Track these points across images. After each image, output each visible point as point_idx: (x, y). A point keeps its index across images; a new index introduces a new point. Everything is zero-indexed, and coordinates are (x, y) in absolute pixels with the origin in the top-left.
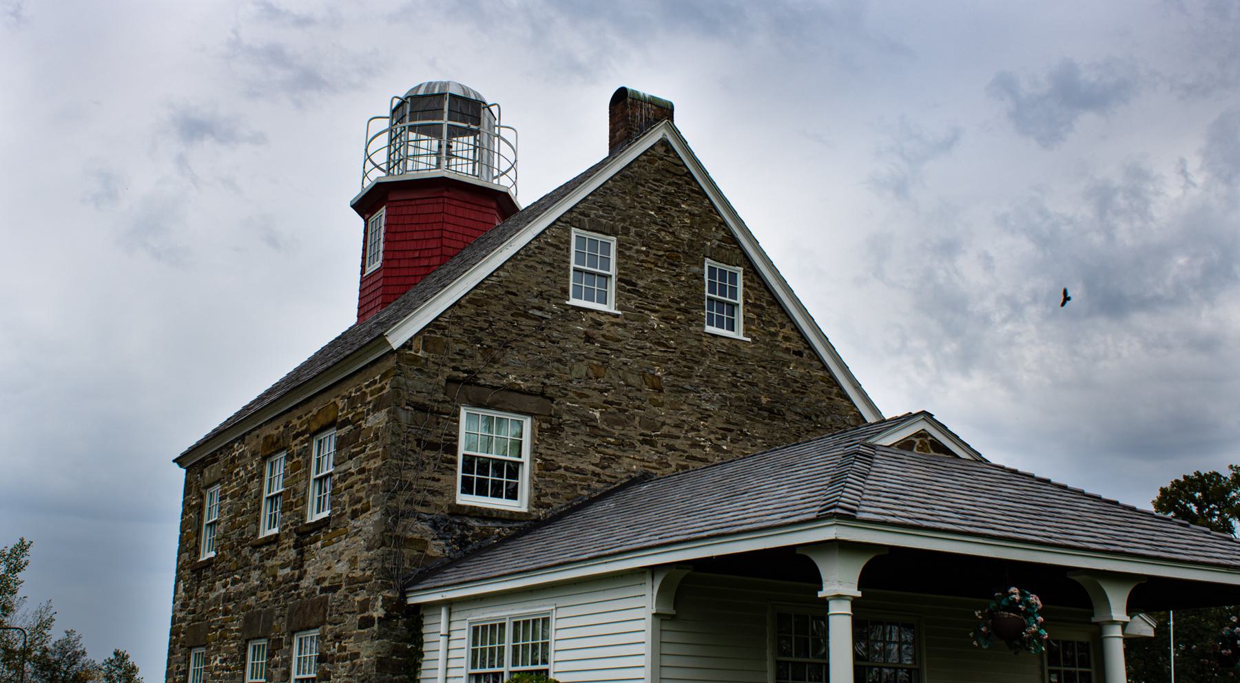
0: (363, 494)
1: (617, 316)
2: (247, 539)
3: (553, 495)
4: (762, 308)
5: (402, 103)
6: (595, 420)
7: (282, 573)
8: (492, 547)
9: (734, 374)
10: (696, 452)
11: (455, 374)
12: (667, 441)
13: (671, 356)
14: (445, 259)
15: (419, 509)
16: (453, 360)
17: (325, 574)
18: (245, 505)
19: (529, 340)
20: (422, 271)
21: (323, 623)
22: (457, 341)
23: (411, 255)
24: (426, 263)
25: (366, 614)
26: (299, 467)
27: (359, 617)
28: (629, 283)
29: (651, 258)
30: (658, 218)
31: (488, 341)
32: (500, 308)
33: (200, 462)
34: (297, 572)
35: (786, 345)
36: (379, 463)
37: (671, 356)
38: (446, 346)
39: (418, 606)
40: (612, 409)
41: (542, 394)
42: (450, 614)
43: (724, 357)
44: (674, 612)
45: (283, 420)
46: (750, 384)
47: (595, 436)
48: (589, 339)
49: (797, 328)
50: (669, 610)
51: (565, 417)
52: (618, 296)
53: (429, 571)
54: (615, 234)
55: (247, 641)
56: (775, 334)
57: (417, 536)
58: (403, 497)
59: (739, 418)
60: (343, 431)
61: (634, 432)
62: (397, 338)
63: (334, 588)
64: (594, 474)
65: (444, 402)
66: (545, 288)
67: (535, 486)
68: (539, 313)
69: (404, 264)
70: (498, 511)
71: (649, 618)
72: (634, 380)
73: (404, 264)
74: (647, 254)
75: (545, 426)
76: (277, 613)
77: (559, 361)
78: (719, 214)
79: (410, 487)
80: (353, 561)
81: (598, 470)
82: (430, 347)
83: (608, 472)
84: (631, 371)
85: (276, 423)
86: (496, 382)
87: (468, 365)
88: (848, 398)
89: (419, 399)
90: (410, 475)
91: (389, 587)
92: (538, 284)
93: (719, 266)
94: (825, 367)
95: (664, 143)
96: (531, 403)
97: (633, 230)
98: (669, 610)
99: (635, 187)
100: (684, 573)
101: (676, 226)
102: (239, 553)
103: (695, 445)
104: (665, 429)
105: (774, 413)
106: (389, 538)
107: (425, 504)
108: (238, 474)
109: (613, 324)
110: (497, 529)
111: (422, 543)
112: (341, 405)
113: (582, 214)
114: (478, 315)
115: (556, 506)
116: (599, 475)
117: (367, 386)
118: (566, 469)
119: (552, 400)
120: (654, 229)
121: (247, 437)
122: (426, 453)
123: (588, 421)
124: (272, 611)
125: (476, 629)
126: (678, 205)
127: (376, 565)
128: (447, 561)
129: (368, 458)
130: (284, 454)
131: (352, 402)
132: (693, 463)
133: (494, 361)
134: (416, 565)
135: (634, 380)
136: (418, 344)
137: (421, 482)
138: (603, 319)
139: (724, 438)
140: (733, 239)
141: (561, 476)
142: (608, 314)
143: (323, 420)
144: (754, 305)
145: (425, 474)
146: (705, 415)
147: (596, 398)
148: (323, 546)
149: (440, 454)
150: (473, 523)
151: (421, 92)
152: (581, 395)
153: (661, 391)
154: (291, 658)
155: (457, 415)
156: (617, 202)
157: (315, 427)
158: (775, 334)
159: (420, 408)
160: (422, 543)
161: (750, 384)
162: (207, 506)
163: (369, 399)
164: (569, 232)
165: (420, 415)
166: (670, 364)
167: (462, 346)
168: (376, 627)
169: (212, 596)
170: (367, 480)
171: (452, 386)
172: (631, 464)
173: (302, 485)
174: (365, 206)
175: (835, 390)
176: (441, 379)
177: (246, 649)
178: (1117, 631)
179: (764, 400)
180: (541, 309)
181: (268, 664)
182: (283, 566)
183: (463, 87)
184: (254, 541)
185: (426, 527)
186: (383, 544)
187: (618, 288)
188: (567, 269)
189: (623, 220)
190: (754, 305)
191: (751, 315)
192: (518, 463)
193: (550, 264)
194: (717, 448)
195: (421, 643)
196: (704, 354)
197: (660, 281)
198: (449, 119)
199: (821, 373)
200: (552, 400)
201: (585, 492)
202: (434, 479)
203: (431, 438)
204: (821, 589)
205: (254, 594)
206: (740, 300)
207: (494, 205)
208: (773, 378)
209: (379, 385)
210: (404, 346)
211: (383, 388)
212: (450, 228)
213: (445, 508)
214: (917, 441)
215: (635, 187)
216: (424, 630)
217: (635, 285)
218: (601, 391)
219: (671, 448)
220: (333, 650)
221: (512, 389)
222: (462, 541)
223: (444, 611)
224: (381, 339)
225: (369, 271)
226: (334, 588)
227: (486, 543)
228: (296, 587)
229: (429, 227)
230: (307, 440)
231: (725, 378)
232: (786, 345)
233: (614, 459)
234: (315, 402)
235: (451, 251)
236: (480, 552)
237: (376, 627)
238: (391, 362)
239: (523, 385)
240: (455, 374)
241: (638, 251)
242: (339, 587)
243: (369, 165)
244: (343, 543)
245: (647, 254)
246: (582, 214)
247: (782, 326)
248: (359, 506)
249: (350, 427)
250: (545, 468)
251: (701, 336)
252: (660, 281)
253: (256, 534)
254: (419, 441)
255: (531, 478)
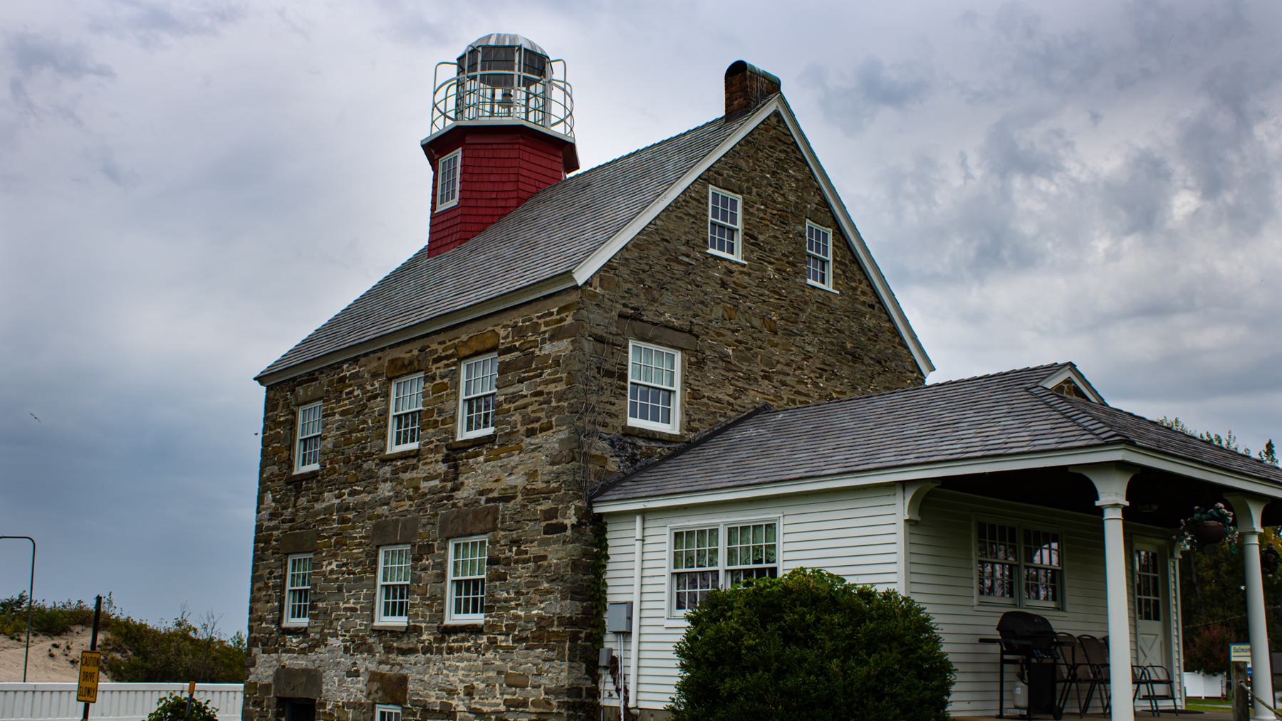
0: (542, 415)
1: (744, 266)
2: (371, 454)
3: (700, 420)
4: (845, 264)
5: (473, 51)
6: (728, 356)
7: (425, 486)
8: (655, 465)
9: (828, 322)
10: (801, 388)
11: (625, 310)
12: (781, 377)
13: (783, 303)
14: (521, 201)
15: (601, 429)
16: (623, 298)
17: (494, 486)
18: (365, 422)
19: (679, 283)
20: (500, 211)
21: (495, 529)
22: (626, 281)
23: (488, 196)
24: (503, 204)
25: (554, 521)
26: (443, 388)
27: (543, 524)
28: (752, 237)
29: (768, 217)
30: (773, 181)
31: (649, 283)
32: (656, 253)
33: (286, 385)
34: (449, 485)
35: (863, 298)
36: (561, 387)
37: (783, 303)
38: (618, 285)
39: (601, 515)
40: (741, 348)
41: (690, 332)
42: (644, 521)
43: (821, 306)
44: (918, 518)
45: (419, 344)
46: (839, 331)
47: (729, 370)
48: (724, 285)
49: (871, 285)
50: (917, 518)
51: (708, 353)
52: (744, 248)
53: (608, 486)
54: (742, 193)
55: (378, 547)
56: (855, 289)
57: (599, 453)
58: (588, 417)
59: (832, 360)
60: (508, 357)
61: (757, 369)
62: (581, 276)
63: (505, 499)
64: (730, 404)
65: (618, 334)
66: (691, 237)
67: (686, 413)
68: (686, 260)
69: (481, 203)
70: (660, 433)
71: (901, 525)
72: (757, 322)
73: (481, 203)
74: (765, 212)
75: (693, 359)
76: (424, 521)
77: (702, 303)
78: (816, 180)
79: (593, 411)
80: (532, 475)
81: (732, 400)
82: (606, 285)
83: (739, 402)
84: (754, 314)
85: (408, 347)
86: (656, 319)
87: (634, 302)
88: (906, 347)
89: (599, 331)
90: (593, 399)
91: (580, 498)
92: (685, 233)
93: (816, 226)
94: (890, 320)
95: (776, 114)
96: (682, 339)
97: (755, 190)
98: (917, 518)
99: (756, 152)
100: (933, 486)
101: (786, 189)
102: (360, 466)
103: (801, 382)
104: (779, 367)
105: (856, 358)
106: (576, 452)
107: (605, 425)
108: (351, 392)
109: (741, 273)
110: (659, 449)
111: (602, 459)
112: (502, 333)
113: (717, 173)
114: (641, 258)
115: (702, 430)
116: (731, 404)
117: (539, 318)
118: (709, 398)
119: (697, 337)
120: (770, 190)
121: (363, 360)
122: (605, 379)
123: (723, 357)
124: (415, 520)
125: (676, 534)
126: (786, 171)
127: (565, 478)
128: (622, 475)
129: (547, 383)
130: (421, 375)
131: (519, 331)
132: (800, 401)
133: (654, 300)
134: (599, 479)
135: (757, 322)
136: (596, 282)
137: (602, 405)
138: (734, 267)
139: (821, 377)
140: (828, 205)
141: (706, 404)
142: (737, 263)
143: (475, 346)
144: (840, 263)
145: (604, 398)
146: (807, 357)
147: (730, 337)
148: (486, 461)
149: (616, 382)
150: (640, 443)
151: (492, 42)
152: (719, 334)
153: (776, 333)
154: (446, 561)
155: (626, 347)
156: (743, 164)
157: (466, 352)
158: (855, 289)
159: (599, 339)
160: (602, 459)
161: (839, 331)
162: (300, 422)
163: (543, 329)
164: (707, 188)
165: (599, 345)
166: (782, 311)
167: (630, 286)
168: (569, 532)
169: (318, 506)
170: (548, 402)
171: (623, 321)
172: (754, 397)
173: (449, 405)
174: (435, 148)
175: (897, 340)
176: (614, 314)
177: (377, 555)
178: (1255, 540)
179: (849, 346)
180: (688, 256)
181: (414, 568)
182: (427, 479)
183: (530, 42)
184: (381, 455)
185: (606, 445)
186: (573, 459)
187: (744, 241)
188: (706, 221)
189: (747, 181)
190: (840, 263)
191: (838, 271)
192: (670, 391)
193: (694, 217)
194: (816, 385)
195: (606, 547)
196: (806, 303)
197: (775, 237)
198: (483, 69)
199: (887, 325)
200: (697, 337)
201: (722, 419)
202: (611, 404)
203: (607, 366)
204: (1097, 499)
205: (388, 504)
206: (830, 257)
207: (561, 154)
208: (855, 327)
209: (555, 317)
210: (586, 283)
211: (562, 320)
212: (525, 173)
213: (620, 429)
214: (1066, 386)
215: (756, 152)
216: (608, 536)
217: (756, 239)
218: (733, 331)
219: (784, 384)
220: (508, 554)
221: (667, 326)
222: (633, 459)
223: (638, 519)
224: (568, 274)
225: (440, 208)
226: (505, 499)
227: (651, 461)
228: (450, 498)
229: (505, 171)
230: (454, 364)
231: (821, 324)
232: (863, 298)
233: (743, 391)
234: (464, 329)
235: (524, 195)
236: (645, 468)
237: (569, 532)
238: (574, 297)
239: (676, 323)
240: (625, 310)
241: (758, 209)
242: (514, 497)
243: (437, 113)
244: (516, 459)
245: (765, 212)
246: (717, 173)
247: (860, 282)
248: (537, 425)
249: (517, 354)
250: (693, 396)
251: (804, 287)
252: (775, 237)
253: (383, 449)
254: (599, 368)
255: (682, 405)
